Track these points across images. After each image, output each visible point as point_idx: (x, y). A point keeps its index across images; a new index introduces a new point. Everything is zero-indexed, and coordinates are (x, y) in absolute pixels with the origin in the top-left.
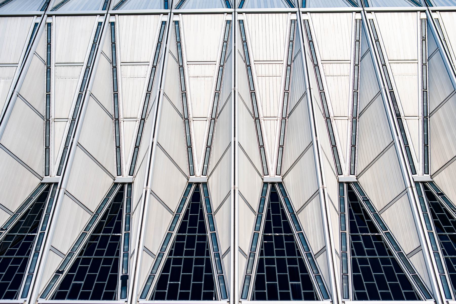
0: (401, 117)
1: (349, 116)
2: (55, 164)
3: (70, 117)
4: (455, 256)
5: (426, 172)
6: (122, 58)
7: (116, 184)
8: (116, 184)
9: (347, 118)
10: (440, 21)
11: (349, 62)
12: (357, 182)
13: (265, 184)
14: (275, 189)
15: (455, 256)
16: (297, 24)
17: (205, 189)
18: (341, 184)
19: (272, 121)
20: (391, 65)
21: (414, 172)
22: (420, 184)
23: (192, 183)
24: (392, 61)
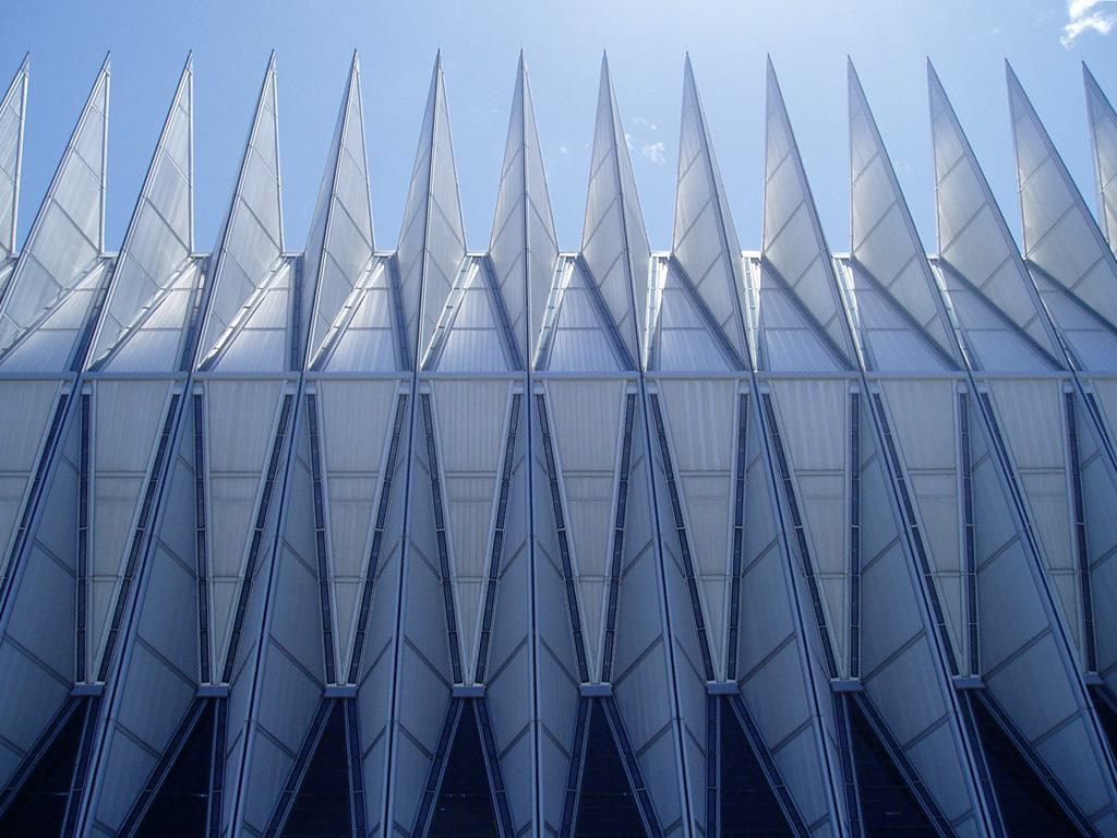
0: (695, 577)
1: (1075, 567)
2: (218, 660)
3: (122, 574)
4: (355, 836)
5: (855, 674)
6: (329, 464)
7: (199, 701)
8: (199, 701)
9: (96, 579)
10: (1096, 399)
11: (98, 474)
12: (738, 695)
13: (454, 701)
14: (730, 707)
15: (355, 836)
16: (751, 401)
17: (482, 708)
18: (710, 698)
19: (473, 585)
20: (686, 480)
21: (955, 671)
22: (966, 693)
23: (459, 698)
24: (799, 471)
